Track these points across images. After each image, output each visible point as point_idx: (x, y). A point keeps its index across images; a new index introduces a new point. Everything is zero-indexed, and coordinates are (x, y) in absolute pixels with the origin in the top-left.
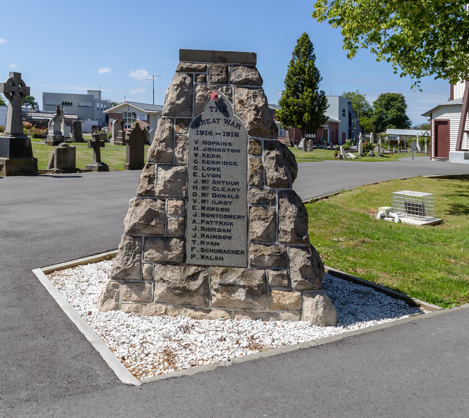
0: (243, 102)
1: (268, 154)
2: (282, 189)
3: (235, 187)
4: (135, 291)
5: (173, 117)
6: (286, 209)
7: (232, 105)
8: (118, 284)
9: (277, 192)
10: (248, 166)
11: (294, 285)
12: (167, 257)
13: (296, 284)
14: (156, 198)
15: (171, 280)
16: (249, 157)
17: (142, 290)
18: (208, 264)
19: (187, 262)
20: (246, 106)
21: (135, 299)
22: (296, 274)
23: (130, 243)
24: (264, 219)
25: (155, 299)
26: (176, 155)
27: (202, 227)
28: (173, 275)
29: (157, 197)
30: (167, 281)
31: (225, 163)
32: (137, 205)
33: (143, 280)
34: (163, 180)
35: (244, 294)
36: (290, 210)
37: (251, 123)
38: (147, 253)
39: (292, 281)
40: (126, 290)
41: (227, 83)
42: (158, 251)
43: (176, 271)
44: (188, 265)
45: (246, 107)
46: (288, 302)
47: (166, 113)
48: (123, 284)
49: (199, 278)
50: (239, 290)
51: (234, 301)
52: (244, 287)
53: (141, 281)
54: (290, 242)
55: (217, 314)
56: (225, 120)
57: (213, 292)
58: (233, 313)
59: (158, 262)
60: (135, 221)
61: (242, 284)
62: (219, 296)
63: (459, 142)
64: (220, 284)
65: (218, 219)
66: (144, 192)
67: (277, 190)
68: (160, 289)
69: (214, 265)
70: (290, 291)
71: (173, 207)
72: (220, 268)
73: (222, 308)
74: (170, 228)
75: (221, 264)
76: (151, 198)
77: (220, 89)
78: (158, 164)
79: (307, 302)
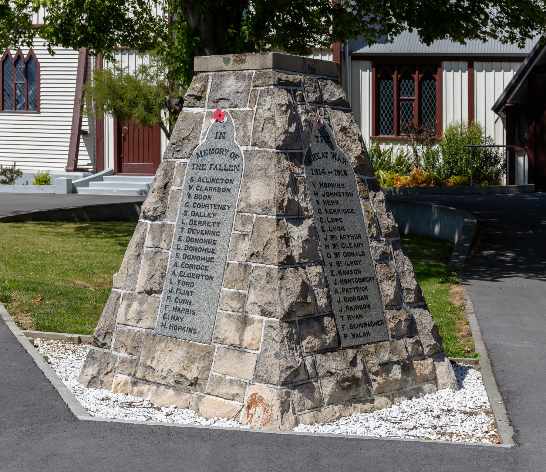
0: (346, 129)
1: (374, 197)
2: (394, 239)
3: (359, 241)
4: (307, 396)
5: (286, 151)
6: (403, 263)
7: (333, 133)
8: (289, 390)
9: (391, 243)
10: (364, 214)
11: (427, 350)
12: (326, 343)
13: (428, 349)
14: (296, 265)
15: (338, 372)
16: (361, 202)
17: (313, 392)
18: (360, 343)
19: (343, 345)
20: (349, 135)
21: (309, 405)
22: (428, 337)
23: (289, 331)
24: (390, 279)
25: (326, 400)
26: (302, 205)
27: (344, 297)
28: (334, 363)
29: (297, 264)
30: (335, 373)
31: (345, 211)
32: (282, 278)
33: (309, 378)
34: (300, 241)
35: (400, 371)
36: (408, 263)
37: (358, 158)
38: (306, 341)
39: (424, 346)
40: (299, 397)
41: (322, 103)
42: (316, 337)
43: (338, 359)
44: (344, 348)
45: (348, 137)
46: (427, 371)
47: (279, 146)
48: (294, 390)
49: (358, 362)
50: (394, 368)
51: (391, 382)
52: (398, 363)
53: (308, 381)
54: (414, 302)
55: (381, 403)
56: (331, 153)
57: (372, 377)
58: (391, 397)
59: (318, 352)
60: (292, 301)
61: (396, 360)
62: (379, 379)
63: (82, 77)
64: (379, 365)
65: (354, 285)
66: (285, 259)
67: (391, 240)
68: (327, 387)
69: (364, 343)
70: (424, 359)
71: (316, 275)
72: (370, 345)
73: (382, 394)
74: (320, 303)
75: (370, 341)
76: (292, 266)
77: (318, 112)
78: (287, 217)
79: (439, 368)
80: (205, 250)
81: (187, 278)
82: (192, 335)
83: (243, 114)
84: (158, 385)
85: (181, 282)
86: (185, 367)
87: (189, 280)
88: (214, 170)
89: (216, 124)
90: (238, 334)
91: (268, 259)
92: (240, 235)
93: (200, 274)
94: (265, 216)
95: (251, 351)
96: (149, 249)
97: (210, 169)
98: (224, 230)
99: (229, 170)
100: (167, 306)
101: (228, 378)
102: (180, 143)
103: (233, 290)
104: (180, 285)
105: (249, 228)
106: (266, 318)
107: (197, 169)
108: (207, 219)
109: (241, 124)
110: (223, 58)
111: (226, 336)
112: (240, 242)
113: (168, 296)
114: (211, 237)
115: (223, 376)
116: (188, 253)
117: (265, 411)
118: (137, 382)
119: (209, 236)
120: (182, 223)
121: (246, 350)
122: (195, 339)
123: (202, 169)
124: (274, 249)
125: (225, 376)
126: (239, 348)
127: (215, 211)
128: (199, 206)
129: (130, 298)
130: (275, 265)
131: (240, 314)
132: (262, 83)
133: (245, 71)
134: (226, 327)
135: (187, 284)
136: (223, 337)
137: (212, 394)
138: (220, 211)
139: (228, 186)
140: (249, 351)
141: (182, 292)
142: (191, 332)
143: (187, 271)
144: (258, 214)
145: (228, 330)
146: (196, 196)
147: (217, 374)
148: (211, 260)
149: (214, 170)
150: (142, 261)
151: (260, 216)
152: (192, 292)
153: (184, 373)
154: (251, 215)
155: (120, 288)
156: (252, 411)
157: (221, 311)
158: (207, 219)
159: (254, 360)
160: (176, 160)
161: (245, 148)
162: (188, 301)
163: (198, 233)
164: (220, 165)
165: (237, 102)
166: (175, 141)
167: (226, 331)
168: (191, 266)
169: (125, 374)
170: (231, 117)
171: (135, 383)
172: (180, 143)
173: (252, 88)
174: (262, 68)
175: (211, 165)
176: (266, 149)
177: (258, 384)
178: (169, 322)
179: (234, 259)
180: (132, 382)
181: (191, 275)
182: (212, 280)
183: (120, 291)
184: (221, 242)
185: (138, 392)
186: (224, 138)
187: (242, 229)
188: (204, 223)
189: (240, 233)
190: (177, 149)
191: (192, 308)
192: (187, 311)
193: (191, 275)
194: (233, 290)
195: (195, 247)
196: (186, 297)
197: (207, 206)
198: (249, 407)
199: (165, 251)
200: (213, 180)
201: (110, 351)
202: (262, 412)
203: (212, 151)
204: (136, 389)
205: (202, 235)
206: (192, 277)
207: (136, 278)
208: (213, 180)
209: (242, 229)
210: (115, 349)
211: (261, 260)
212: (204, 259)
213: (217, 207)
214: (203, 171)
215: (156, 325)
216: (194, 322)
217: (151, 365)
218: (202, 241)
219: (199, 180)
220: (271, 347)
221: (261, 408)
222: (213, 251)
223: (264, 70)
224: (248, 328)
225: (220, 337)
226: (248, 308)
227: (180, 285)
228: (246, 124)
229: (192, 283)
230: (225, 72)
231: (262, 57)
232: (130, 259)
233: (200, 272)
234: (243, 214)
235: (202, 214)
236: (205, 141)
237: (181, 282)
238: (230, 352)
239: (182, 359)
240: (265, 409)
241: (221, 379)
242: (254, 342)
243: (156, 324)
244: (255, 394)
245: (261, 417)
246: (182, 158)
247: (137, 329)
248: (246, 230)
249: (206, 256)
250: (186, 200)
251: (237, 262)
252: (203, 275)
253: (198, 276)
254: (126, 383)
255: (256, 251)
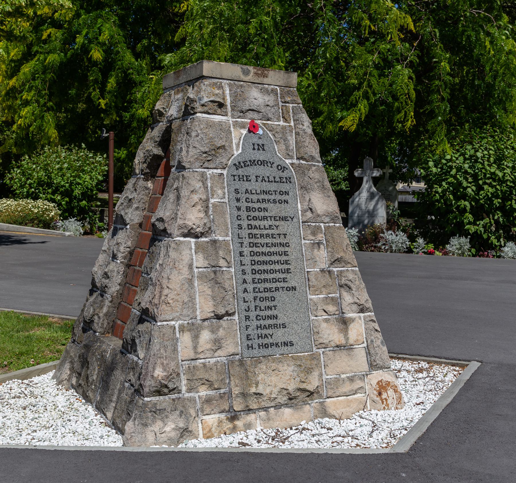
80: (278, 262)
81: (264, 293)
82: (289, 348)
83: (280, 128)
84: (266, 409)
85: (258, 299)
86: (303, 380)
87: (267, 295)
88: (262, 181)
89: (250, 135)
90: (342, 334)
91: (349, 263)
92: (314, 244)
93: (279, 286)
94: (333, 224)
95: (357, 346)
96: (200, 270)
97: (257, 181)
98: (293, 241)
99: (281, 182)
100: (247, 327)
101: (343, 376)
102: (213, 152)
103: (323, 296)
104: (258, 301)
105: (321, 237)
106: (362, 315)
107: (239, 180)
108: (270, 232)
109: (281, 138)
110: (242, 68)
111: (330, 339)
112: (316, 250)
113: (246, 316)
114: (282, 249)
115: (338, 376)
116: (257, 267)
117: (395, 392)
118: (236, 415)
119: (277, 248)
120: (239, 238)
121: (352, 347)
122: (293, 351)
123: (247, 180)
124: (350, 253)
125: (340, 376)
126: (345, 348)
127: (277, 223)
128: (255, 218)
129: (194, 330)
130: (356, 267)
131: (337, 316)
132: (291, 100)
133: (267, 86)
134: (328, 332)
135: (266, 299)
136: (328, 341)
137: (334, 395)
138: (282, 223)
139: (284, 197)
140: (355, 347)
141: (263, 308)
142: (287, 345)
143: (262, 286)
144: (325, 223)
145: (331, 334)
146: (248, 209)
147: (332, 377)
148: (288, 271)
149: (262, 181)
150: (196, 284)
151: (327, 224)
152: (275, 306)
153: (303, 386)
154: (317, 224)
155: (172, 320)
156: (384, 396)
157: (315, 318)
158: (270, 232)
159: (363, 353)
160: (206, 170)
161: (290, 161)
162: (274, 316)
163: (263, 247)
164: (268, 177)
165: (270, 116)
166: (207, 150)
167: (329, 334)
168: (265, 280)
169: (215, 414)
170: (266, 130)
171: (233, 418)
172: (213, 152)
173: (281, 104)
174: (286, 85)
175: (256, 177)
176: (314, 163)
177: (374, 372)
178: (256, 342)
179: (314, 268)
180: (228, 418)
181: (266, 290)
182: (295, 290)
183: (173, 323)
184: (294, 253)
185: (244, 425)
186: (264, 150)
187: (313, 238)
188: (267, 236)
189: (312, 242)
190: (209, 159)
191: (279, 322)
192: (275, 326)
193: (266, 290)
194: (323, 296)
195: (263, 261)
196: (269, 313)
197: (265, 218)
198: (380, 394)
199: (224, 269)
200: (264, 192)
201: (181, 395)
202: (394, 393)
203: (253, 163)
204: (239, 423)
205: (268, 248)
206: (270, 291)
207: (194, 304)
208: (264, 192)
209: (313, 238)
210: (189, 390)
211: (343, 264)
212: (279, 271)
213: (278, 218)
214: (249, 183)
215: (240, 349)
216: (287, 335)
217: (258, 391)
218: (270, 254)
219: (247, 191)
220: (375, 338)
221: (391, 390)
222: (286, 262)
223: (287, 88)
224: (352, 326)
225: (324, 342)
226: (346, 309)
227: (258, 301)
228: (286, 138)
229: (271, 297)
230: (242, 83)
231: (286, 75)
232: (183, 284)
233: (278, 285)
234: (309, 224)
235: (262, 227)
236: (240, 151)
237: (258, 299)
238: (337, 353)
239: (295, 374)
240: (394, 390)
241: (337, 380)
242: (360, 338)
243: (240, 348)
244: (381, 381)
245: (395, 398)
246: (215, 168)
247: (212, 361)
248: (318, 239)
249: (280, 268)
250: (236, 213)
251: (318, 270)
252: (283, 288)
253: (277, 289)
254: (220, 422)
255: (339, 257)
